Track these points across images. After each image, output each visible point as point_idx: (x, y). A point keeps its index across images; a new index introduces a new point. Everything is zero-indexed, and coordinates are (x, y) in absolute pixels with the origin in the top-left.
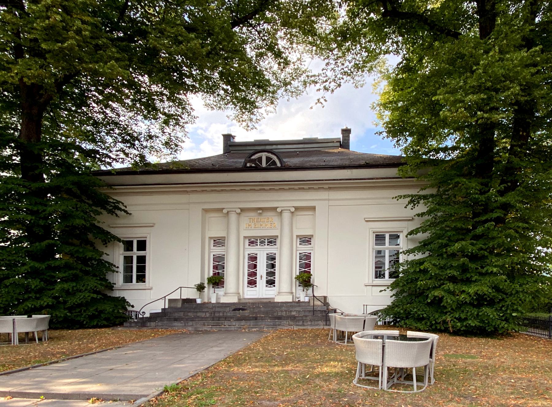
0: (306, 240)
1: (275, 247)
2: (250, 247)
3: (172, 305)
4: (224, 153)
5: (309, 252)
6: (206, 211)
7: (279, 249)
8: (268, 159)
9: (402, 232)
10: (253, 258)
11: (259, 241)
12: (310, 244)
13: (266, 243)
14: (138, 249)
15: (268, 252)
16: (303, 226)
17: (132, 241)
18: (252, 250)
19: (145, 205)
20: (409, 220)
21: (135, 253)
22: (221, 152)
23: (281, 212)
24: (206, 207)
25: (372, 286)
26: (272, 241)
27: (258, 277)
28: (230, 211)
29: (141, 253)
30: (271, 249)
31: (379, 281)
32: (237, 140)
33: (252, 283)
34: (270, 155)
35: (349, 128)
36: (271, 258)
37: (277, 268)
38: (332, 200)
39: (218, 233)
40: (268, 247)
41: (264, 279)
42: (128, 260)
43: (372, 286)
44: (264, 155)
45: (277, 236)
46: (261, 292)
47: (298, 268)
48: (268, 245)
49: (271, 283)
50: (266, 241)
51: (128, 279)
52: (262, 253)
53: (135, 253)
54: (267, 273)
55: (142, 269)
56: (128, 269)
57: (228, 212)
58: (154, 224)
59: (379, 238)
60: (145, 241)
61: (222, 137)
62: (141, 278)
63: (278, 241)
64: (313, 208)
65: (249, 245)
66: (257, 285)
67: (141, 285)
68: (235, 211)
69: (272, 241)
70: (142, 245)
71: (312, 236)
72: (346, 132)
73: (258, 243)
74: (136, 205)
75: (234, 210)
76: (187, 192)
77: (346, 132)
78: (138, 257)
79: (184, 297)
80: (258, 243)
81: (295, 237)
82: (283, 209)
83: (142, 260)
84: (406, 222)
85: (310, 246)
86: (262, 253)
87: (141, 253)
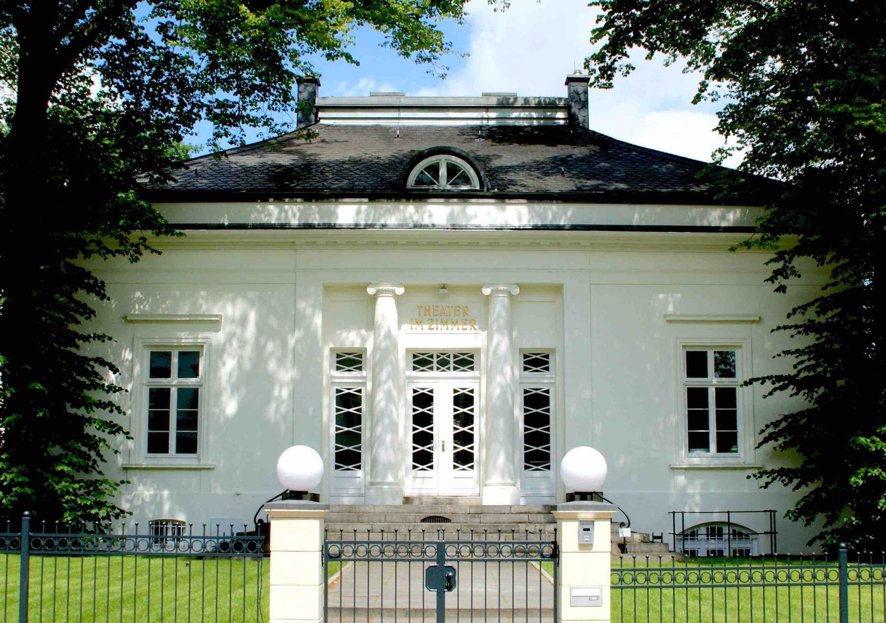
8: (452, 170)
9: (740, 347)
10: (423, 400)
13: (452, 365)
14: (181, 374)
17: (705, 353)
18: (426, 380)
20: (754, 321)
21: (712, 382)
24: (526, 279)
26: (465, 361)
27: (436, 443)
30: (462, 380)
31: (699, 458)
34: (454, 159)
36: (463, 400)
37: (365, 424)
40: (457, 374)
41: (450, 453)
42: (159, 398)
44: (443, 160)
46: (444, 481)
48: (438, 369)
51: (157, 444)
52: (443, 386)
53: (174, 382)
54: (338, 436)
55: (189, 421)
56: (158, 421)
59: (696, 363)
62: (188, 445)
64: (558, 289)
66: (434, 463)
67: (187, 460)
69: (465, 361)
70: (190, 362)
73: (435, 365)
78: (719, 391)
80: (435, 365)
83: (191, 398)
84: (748, 326)
86: (443, 386)
87: (697, 382)
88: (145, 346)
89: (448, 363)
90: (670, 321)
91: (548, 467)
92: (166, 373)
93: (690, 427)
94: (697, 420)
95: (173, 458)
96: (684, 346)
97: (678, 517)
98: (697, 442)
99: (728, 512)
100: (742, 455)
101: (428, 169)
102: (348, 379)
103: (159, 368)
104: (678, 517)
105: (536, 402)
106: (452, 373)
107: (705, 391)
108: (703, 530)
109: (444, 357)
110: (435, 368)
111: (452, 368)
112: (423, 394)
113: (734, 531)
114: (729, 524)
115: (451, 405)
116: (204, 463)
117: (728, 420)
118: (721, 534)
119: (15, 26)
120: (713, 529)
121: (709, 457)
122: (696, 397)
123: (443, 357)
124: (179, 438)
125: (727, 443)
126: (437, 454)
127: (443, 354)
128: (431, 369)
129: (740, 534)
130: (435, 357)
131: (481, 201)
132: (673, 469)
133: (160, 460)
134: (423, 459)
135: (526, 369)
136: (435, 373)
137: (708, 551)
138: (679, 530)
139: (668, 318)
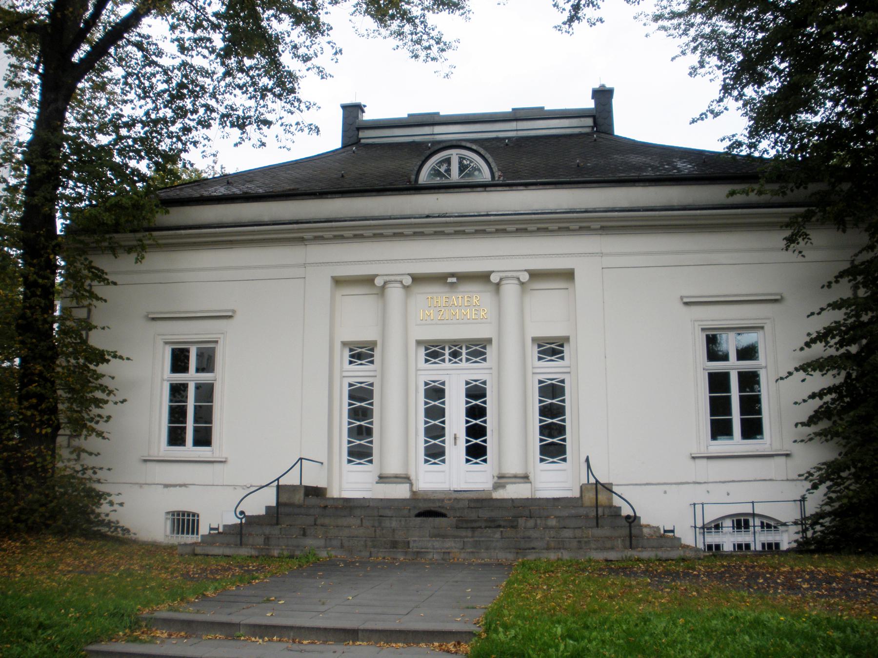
0: (552, 349)
1: (484, 365)
2: (428, 366)
3: (284, 499)
4: (345, 145)
5: (561, 377)
6: (338, 282)
7: (530, 371)
9: (762, 328)
10: (436, 392)
11: (447, 352)
12: (562, 358)
13: (464, 356)
15: (470, 377)
16: (547, 313)
17: (188, 351)
19: (249, 268)
21: (733, 367)
22: (338, 145)
23: (498, 285)
25: (709, 458)
26: (477, 350)
27: (448, 437)
28: (390, 282)
29: (180, 377)
31: (722, 446)
32: (369, 115)
33: (435, 453)
35: (608, 86)
36: (476, 392)
38: (608, 255)
39: (362, 331)
41: (462, 445)
43: (709, 458)
44: (454, 155)
45: (490, 341)
47: (345, 438)
48: (467, 360)
49: (476, 452)
50: (464, 351)
51: (176, 438)
52: (456, 378)
53: (192, 377)
55: (204, 415)
57: (385, 283)
58: (234, 311)
60: (213, 350)
61: (341, 111)
62: (203, 439)
63: (377, 353)
64: (568, 275)
65: (427, 361)
66: (447, 457)
67: (202, 452)
68: (401, 282)
69: (477, 350)
70: (207, 363)
71: (567, 339)
72: (603, 96)
73: (447, 357)
74: (193, 270)
75: (398, 278)
76: (302, 240)
77: (603, 96)
79: (306, 483)
80: (447, 357)
81: (412, 345)
82: (387, 278)
83: (206, 392)
85: (560, 363)
88: (166, 343)
89: (461, 354)
90: (686, 304)
91: (564, 460)
92: (185, 369)
93: (712, 413)
94: (719, 406)
95: (189, 450)
96: (703, 329)
97: (699, 508)
98: (720, 429)
99: (753, 503)
100: (768, 442)
101: (441, 163)
102: (551, 370)
103: (179, 361)
104: (699, 508)
105: (552, 391)
106: (464, 364)
107: (726, 376)
108: (728, 523)
109: (456, 348)
110: (447, 360)
111: (464, 360)
112: (476, 458)
113: (762, 523)
114: (754, 515)
115: (463, 398)
116: (217, 456)
117: (751, 405)
118: (747, 525)
119: (72, 55)
120: (739, 522)
121: (736, 443)
122: (718, 382)
123: (455, 348)
124: (196, 430)
125: (752, 429)
126: (448, 446)
127: (455, 346)
128: (443, 361)
129: (769, 526)
130: (464, 348)
131: (463, 190)
132: (694, 458)
133: (177, 452)
134: (435, 453)
135: (540, 359)
136: (447, 365)
137: (734, 545)
138: (699, 524)
139: (686, 300)
